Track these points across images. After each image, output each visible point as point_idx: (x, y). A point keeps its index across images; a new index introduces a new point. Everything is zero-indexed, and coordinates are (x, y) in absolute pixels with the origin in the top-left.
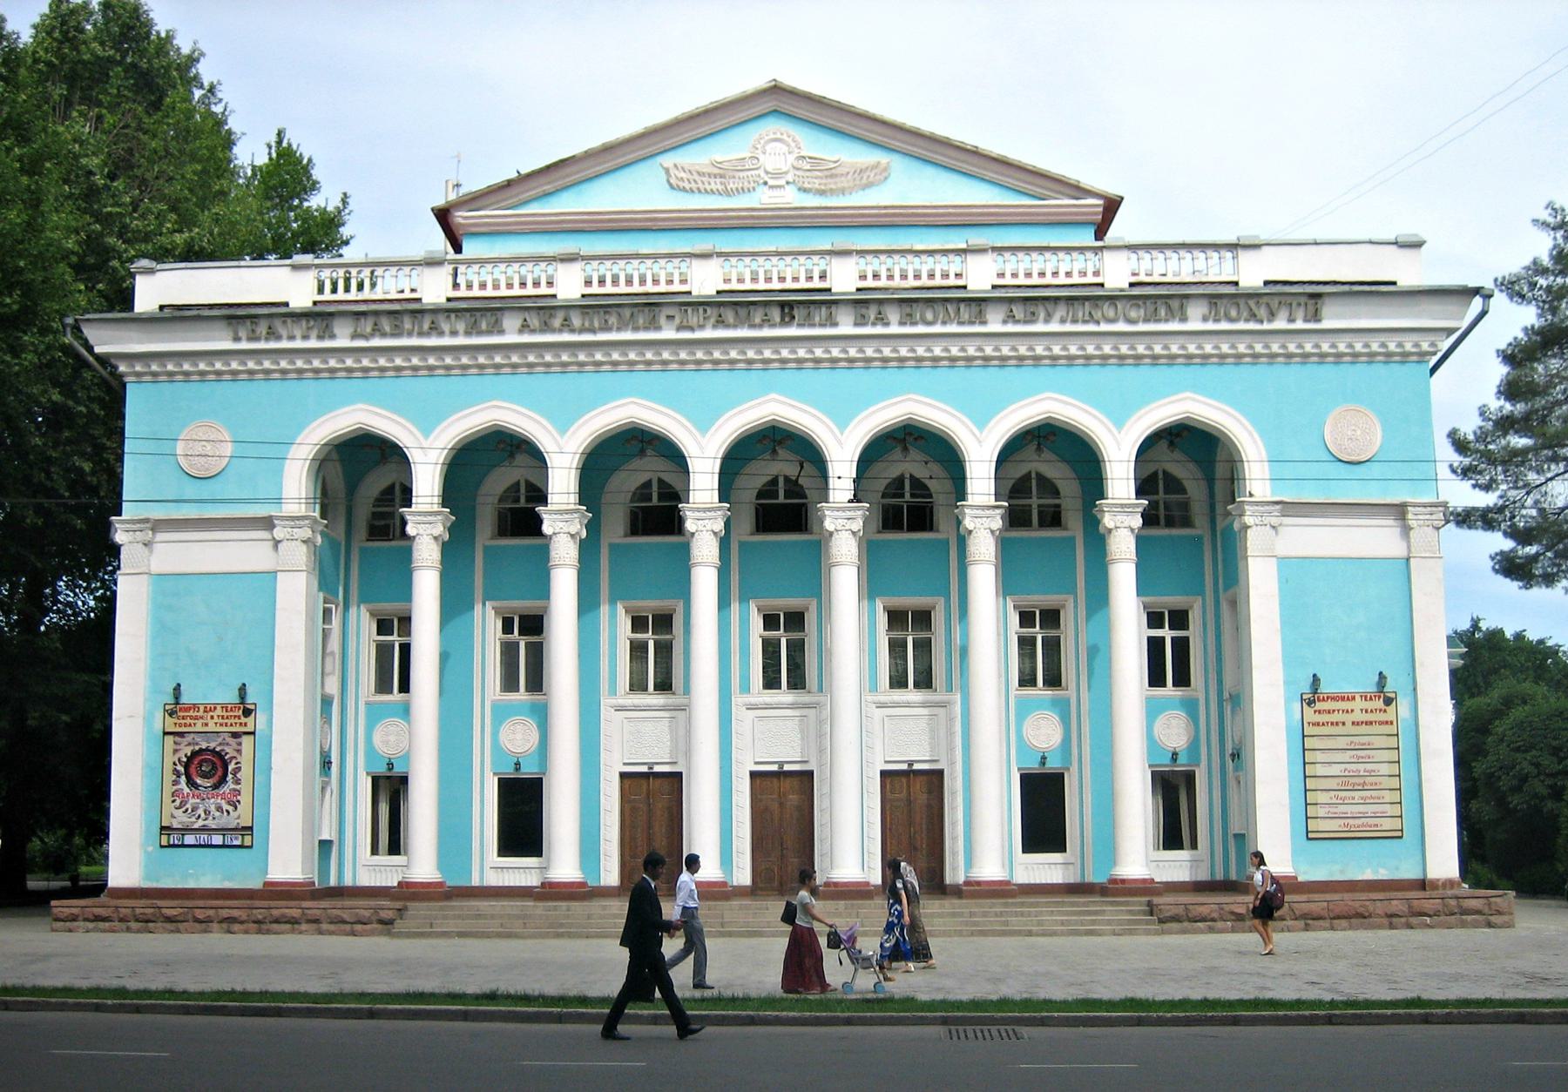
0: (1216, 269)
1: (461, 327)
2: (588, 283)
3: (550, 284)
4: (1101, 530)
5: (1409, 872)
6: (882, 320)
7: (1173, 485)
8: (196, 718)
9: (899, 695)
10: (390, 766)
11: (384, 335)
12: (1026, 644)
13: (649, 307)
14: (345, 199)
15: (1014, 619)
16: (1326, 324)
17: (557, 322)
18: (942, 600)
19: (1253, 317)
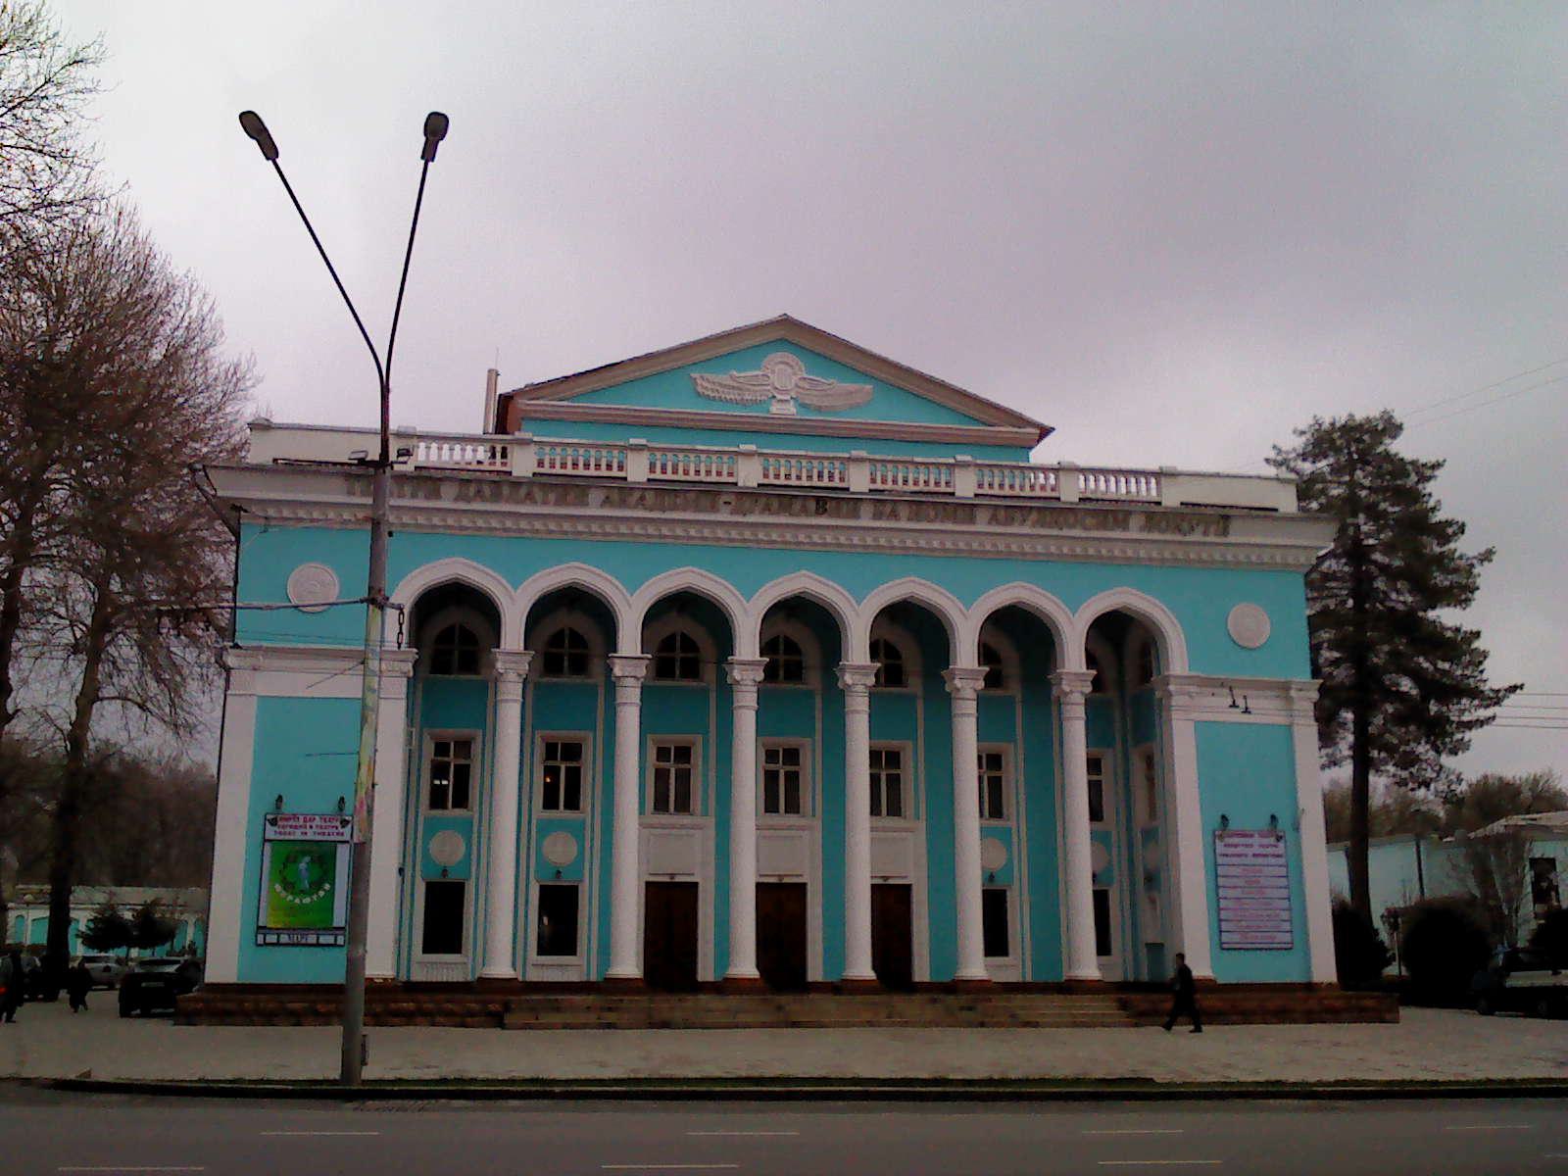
0: (1148, 491)
1: (552, 497)
2: (541, 464)
3: (621, 468)
4: (840, 685)
5: (1296, 977)
6: (894, 515)
7: (792, 647)
8: (296, 827)
9: (664, 818)
10: (445, 872)
11: (484, 499)
12: (661, 776)
13: (709, 493)
14: (1445, 461)
15: (652, 754)
16: (1231, 539)
17: (472, 490)
18: (910, 743)
19: (1179, 530)
